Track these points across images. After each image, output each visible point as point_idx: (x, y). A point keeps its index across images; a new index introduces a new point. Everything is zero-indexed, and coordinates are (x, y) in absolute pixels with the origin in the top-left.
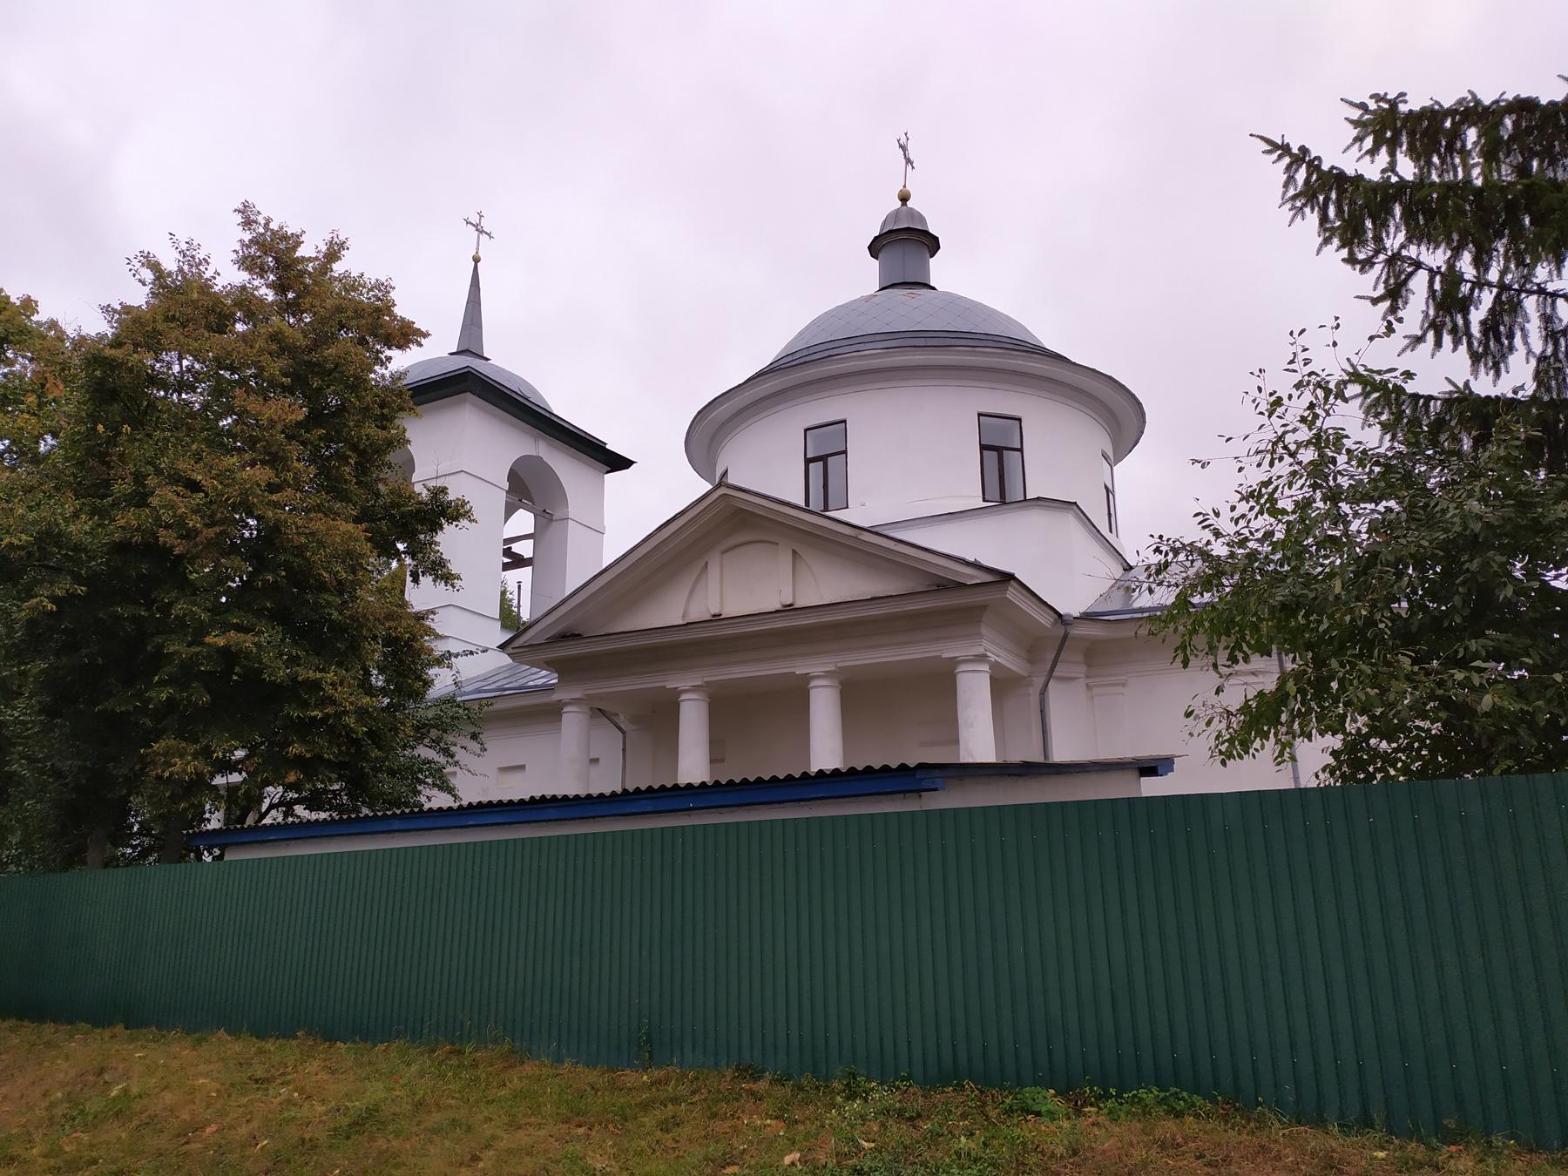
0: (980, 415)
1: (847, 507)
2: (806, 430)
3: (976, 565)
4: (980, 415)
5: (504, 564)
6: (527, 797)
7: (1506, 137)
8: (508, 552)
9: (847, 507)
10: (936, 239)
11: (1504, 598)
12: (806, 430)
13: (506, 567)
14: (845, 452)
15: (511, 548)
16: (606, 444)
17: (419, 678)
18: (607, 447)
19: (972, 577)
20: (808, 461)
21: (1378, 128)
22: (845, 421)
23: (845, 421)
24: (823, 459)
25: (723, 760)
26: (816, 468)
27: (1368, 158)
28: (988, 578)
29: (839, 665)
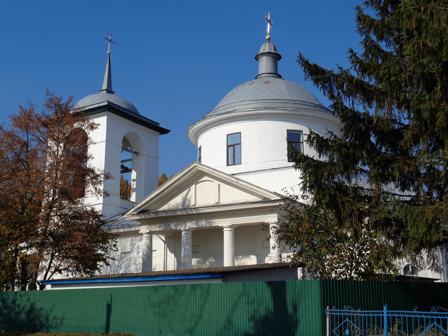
0: (228, 165)
1: (241, 164)
2: (227, 135)
3: (275, 193)
4: (228, 165)
5: (121, 171)
6: (287, 150)
7: (63, 202)
8: (122, 166)
11: (374, 125)
12: (227, 135)
13: (122, 172)
14: (240, 144)
15: (123, 165)
19: (273, 197)
20: (228, 146)
21: (304, 175)
24: (233, 146)
25: (198, 252)
26: (231, 149)
28: (280, 198)
29: (233, 224)
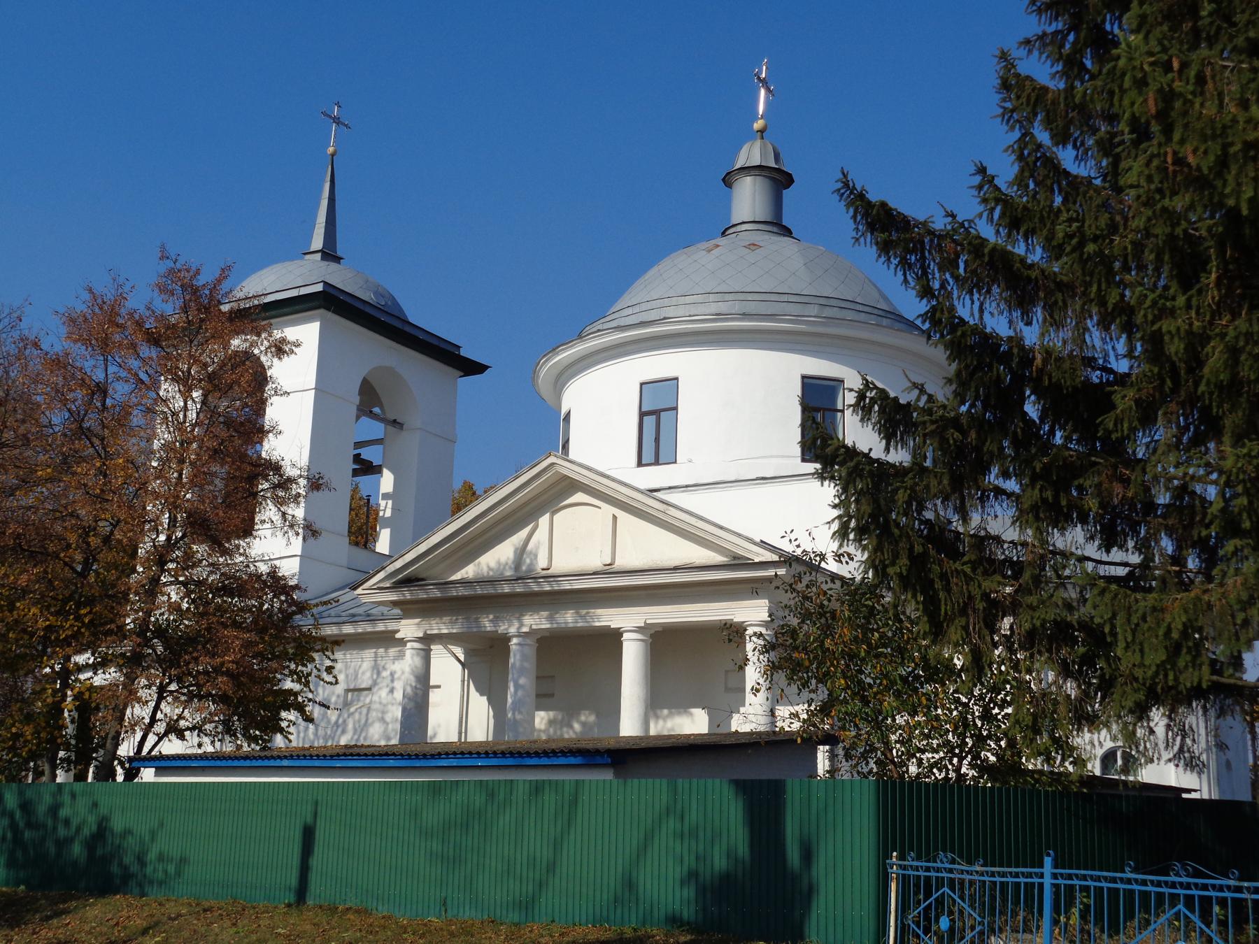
1: (675, 462)
2: (642, 384)
3: (763, 544)
8: (357, 458)
9: (675, 462)
10: (790, 175)
12: (642, 384)
13: (356, 473)
14: (676, 409)
15: (360, 454)
16: (459, 347)
17: (416, 694)
18: (463, 353)
19: (758, 554)
20: (642, 415)
22: (677, 379)
23: (677, 379)
24: (656, 413)
25: (552, 695)
26: (650, 421)
27: (309, 820)
28: (776, 558)
